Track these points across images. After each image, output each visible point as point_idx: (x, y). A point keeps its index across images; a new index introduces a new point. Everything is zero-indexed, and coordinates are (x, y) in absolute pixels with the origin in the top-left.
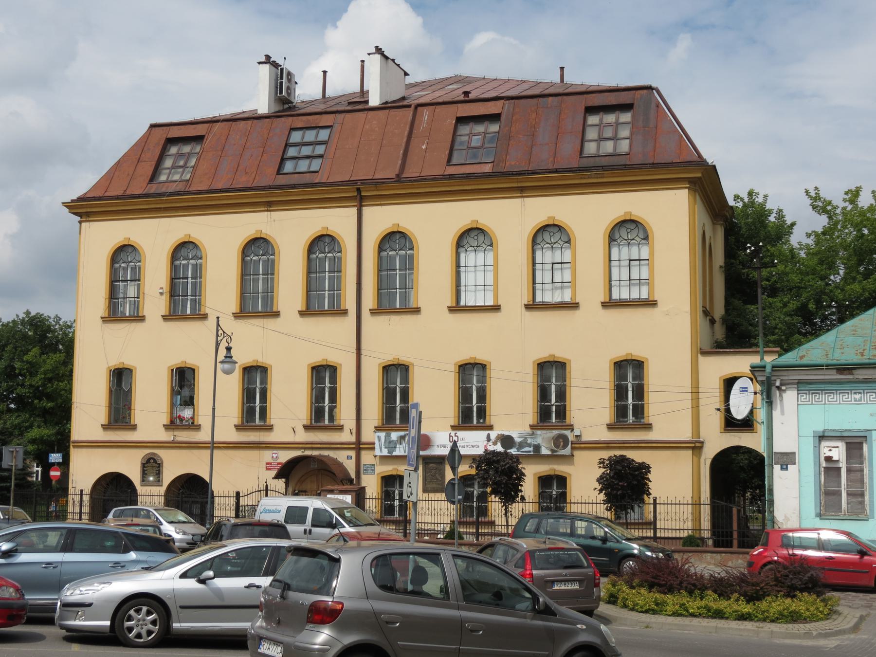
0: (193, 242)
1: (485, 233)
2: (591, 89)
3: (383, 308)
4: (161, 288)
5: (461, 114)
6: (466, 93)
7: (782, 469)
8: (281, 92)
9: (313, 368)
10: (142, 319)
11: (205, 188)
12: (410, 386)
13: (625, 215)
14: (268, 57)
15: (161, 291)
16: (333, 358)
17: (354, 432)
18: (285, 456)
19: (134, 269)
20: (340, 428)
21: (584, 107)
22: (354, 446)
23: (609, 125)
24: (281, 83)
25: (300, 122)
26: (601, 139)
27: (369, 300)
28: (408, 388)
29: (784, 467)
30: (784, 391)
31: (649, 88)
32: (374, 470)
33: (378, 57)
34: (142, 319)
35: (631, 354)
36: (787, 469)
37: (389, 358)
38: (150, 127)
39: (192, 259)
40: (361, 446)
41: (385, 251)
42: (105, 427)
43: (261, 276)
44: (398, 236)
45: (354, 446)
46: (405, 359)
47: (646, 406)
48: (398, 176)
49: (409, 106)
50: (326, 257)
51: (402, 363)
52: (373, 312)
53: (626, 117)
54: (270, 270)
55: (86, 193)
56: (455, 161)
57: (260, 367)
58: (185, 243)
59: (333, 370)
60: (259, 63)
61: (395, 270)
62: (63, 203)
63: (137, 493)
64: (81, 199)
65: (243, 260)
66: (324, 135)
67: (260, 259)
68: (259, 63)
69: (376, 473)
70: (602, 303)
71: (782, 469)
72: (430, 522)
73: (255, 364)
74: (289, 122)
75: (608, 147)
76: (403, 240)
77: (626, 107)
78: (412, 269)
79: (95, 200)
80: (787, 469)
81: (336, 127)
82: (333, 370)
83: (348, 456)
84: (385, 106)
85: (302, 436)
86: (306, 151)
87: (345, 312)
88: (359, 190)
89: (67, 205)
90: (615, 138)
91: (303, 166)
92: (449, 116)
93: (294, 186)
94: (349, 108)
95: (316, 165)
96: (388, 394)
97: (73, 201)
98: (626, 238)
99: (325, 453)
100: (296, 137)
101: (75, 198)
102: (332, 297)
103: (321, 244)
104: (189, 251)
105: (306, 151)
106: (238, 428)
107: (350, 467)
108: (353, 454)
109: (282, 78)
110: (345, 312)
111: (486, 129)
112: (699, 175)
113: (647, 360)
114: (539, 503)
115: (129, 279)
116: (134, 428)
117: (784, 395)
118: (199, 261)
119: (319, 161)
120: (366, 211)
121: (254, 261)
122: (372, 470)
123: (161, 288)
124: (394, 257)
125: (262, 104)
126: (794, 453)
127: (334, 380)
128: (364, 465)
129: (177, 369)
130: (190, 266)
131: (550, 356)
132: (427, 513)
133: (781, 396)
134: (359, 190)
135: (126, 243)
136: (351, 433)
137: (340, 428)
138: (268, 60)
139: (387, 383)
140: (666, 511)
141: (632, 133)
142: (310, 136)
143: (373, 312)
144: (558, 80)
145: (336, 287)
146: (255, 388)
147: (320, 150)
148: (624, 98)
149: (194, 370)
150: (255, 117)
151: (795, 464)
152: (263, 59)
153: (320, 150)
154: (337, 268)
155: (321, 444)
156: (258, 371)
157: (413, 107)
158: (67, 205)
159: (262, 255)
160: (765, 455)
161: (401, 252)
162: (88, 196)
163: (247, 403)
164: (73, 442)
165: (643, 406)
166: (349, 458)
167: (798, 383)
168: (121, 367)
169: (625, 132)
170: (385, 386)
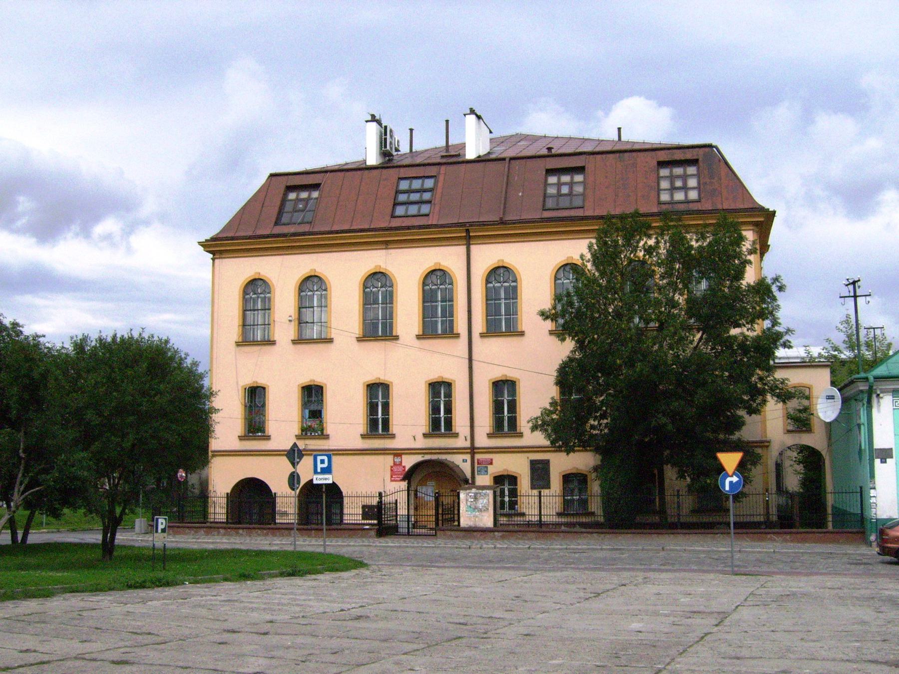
0: (262, 280)
1: (387, 276)
2: (637, 147)
3: (493, 330)
4: (290, 316)
5: (549, 167)
6: (549, 149)
7: (882, 462)
8: (386, 147)
9: (430, 384)
10: (272, 343)
11: (250, 233)
12: (517, 398)
13: (567, 260)
14: (373, 116)
15: (290, 318)
16: (447, 376)
17: (469, 438)
18: (409, 462)
19: (264, 300)
20: (456, 435)
21: (285, 186)
22: (469, 451)
23: (678, 177)
24: (386, 139)
25: (403, 172)
26: (685, 188)
27: (479, 325)
28: (515, 400)
29: (883, 461)
30: (882, 398)
31: (710, 146)
32: (487, 471)
33: (473, 117)
34: (272, 343)
35: (506, 376)
36: (885, 462)
37: (498, 373)
38: (269, 177)
39: (317, 291)
40: (475, 451)
41: (428, 285)
42: (241, 438)
43: (380, 305)
44: (502, 270)
45: (469, 451)
46: (511, 375)
47: (518, 417)
48: (501, 219)
49: (504, 159)
50: (386, 290)
51: (446, 380)
52: (482, 335)
53: (692, 170)
54: (389, 298)
55: (218, 234)
56: (285, 219)
57: (382, 384)
58: (311, 276)
59: (448, 385)
60: (367, 121)
61: (379, 304)
62: (199, 242)
63: (342, 495)
64: (213, 239)
65: (244, 297)
66: (429, 183)
67: (379, 291)
68: (367, 121)
69: (489, 473)
70: (417, 336)
71: (882, 462)
72: (548, 514)
73: (378, 382)
74: (393, 173)
75: (679, 196)
76: (506, 273)
77: (694, 162)
78: (517, 298)
79: (227, 240)
80: (885, 462)
81: (441, 178)
82: (448, 385)
83: (463, 460)
84: (479, 160)
85: (421, 443)
86: (415, 197)
87: (457, 336)
88: (468, 231)
89: (201, 244)
90: (685, 188)
91: (413, 209)
92: (651, 160)
93: (408, 228)
94: (444, 160)
95: (425, 209)
96: (498, 407)
97: (207, 241)
98: (312, 289)
99: (443, 457)
100: (404, 185)
101: (208, 238)
102: (508, 321)
103: (434, 277)
104: (314, 283)
105: (415, 197)
106: (363, 436)
107: (466, 468)
108: (468, 457)
109: (386, 134)
110: (457, 336)
111: (572, 178)
112: (762, 219)
113: (364, 383)
114: (564, 496)
115: (259, 308)
116: (268, 438)
117: (881, 401)
118: (268, 295)
119: (429, 206)
120: (474, 248)
121: (389, 291)
122: (486, 471)
123: (290, 316)
124: (436, 291)
125: (373, 159)
126: (891, 449)
127: (449, 395)
128: (487, 467)
129: (250, 387)
130: (380, 292)
131: (503, 375)
132: (533, 507)
133: (879, 402)
134: (468, 231)
135: (257, 277)
136: (466, 440)
137: (456, 435)
138: (374, 119)
139: (370, 399)
140: (548, 501)
141: (699, 183)
142: (416, 184)
143: (482, 335)
144: (616, 139)
145: (449, 313)
146: (378, 403)
147: (427, 196)
148: (310, 180)
149: (264, 388)
150: (362, 168)
151: (892, 457)
152: (370, 118)
153: (427, 196)
154: (449, 299)
155: (536, 448)
156: (506, 385)
157: (507, 160)
158: (201, 244)
159: (381, 287)
160: (824, 453)
161: (441, 287)
162: (221, 236)
163: (432, 415)
164: (212, 452)
165: (515, 418)
166: (465, 461)
167: (893, 391)
168: (255, 385)
169: (692, 182)
170: (431, 400)
